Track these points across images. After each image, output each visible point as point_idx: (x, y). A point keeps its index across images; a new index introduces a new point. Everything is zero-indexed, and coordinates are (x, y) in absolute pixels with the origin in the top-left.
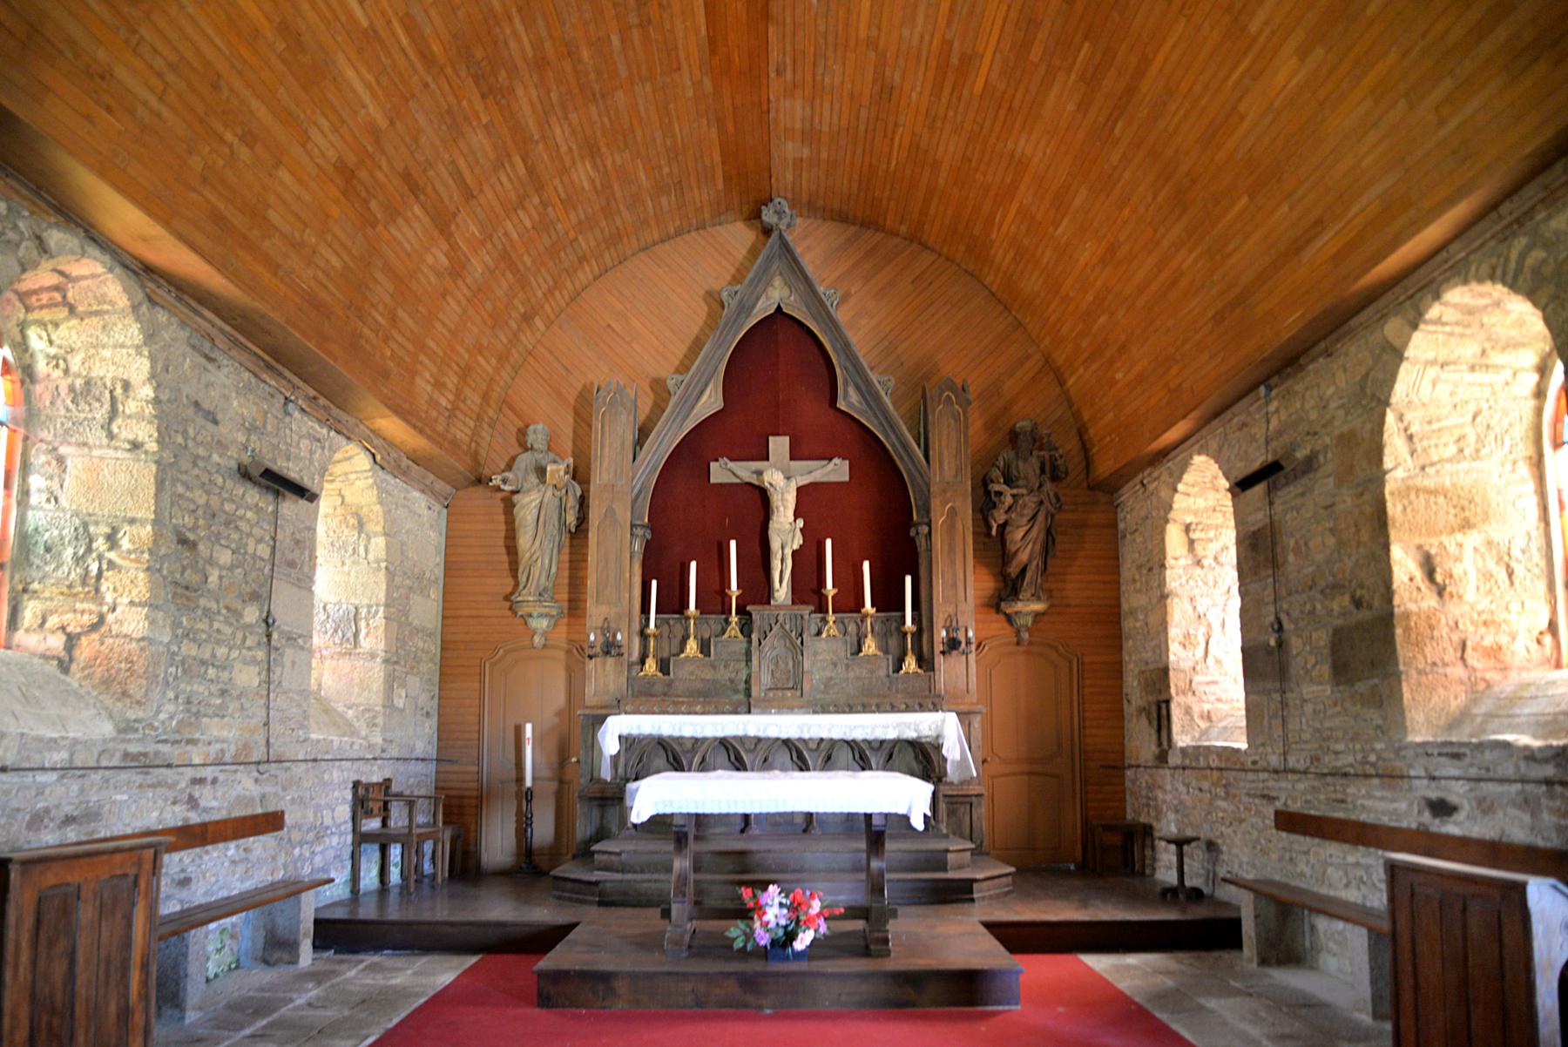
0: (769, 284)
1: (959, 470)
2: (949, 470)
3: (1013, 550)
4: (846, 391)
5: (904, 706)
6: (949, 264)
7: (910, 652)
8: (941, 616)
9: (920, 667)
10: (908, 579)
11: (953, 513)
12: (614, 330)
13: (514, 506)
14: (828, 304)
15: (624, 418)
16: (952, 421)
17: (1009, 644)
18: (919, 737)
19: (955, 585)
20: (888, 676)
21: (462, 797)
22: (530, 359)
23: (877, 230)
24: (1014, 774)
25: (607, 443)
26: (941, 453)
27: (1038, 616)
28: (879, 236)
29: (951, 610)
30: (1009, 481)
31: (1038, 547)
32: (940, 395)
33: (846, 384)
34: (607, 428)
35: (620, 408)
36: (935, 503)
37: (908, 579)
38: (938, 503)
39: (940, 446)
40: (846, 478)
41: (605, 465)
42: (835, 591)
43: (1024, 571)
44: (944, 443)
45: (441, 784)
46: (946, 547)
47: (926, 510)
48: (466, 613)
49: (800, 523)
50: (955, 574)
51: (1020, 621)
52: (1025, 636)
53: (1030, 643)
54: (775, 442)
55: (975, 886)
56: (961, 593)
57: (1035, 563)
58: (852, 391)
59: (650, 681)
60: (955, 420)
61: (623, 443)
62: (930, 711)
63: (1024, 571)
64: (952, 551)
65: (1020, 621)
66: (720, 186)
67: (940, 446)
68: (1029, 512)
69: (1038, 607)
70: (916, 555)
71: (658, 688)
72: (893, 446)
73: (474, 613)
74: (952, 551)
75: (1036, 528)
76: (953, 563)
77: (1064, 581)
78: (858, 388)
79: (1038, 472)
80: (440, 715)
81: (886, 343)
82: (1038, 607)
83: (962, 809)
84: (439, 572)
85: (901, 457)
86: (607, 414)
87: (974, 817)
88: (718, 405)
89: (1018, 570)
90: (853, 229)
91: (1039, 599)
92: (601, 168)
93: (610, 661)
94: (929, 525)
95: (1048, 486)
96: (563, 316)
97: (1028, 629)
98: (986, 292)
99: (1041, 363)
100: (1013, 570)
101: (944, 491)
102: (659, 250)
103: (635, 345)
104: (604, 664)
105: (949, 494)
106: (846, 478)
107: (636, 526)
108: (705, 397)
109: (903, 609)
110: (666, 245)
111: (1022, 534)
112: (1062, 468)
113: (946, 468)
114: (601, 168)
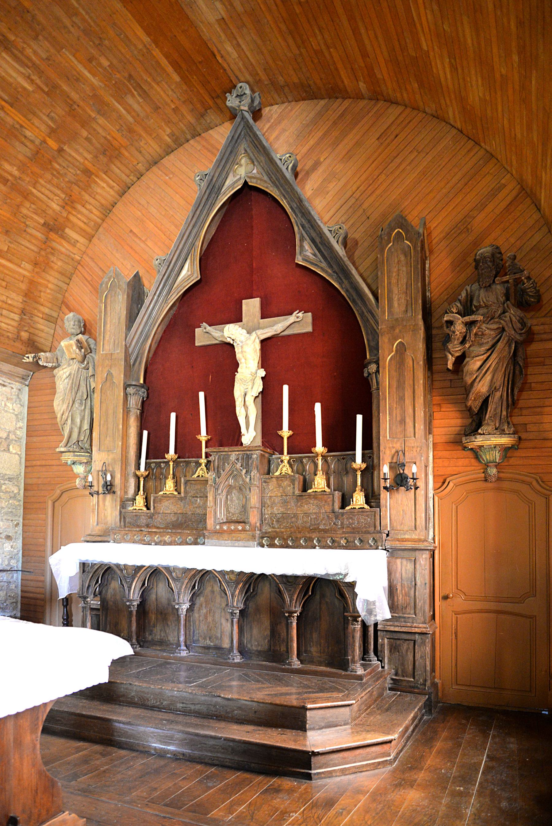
0: (235, 162)
1: (409, 305)
2: (398, 307)
3: (469, 382)
4: (302, 246)
5: (343, 542)
6: (415, 112)
7: (358, 488)
8: (388, 452)
9: (367, 502)
10: (359, 418)
11: (402, 348)
12: (134, 234)
13: (54, 376)
14: (284, 169)
15: (120, 297)
16: (402, 258)
17: (475, 481)
18: (327, 574)
19: (403, 421)
20: (333, 512)
21: (36, 599)
22: (80, 267)
23: (344, 98)
24: (481, 611)
25: (108, 320)
26: (390, 291)
27: (506, 450)
28: (347, 103)
29: (398, 446)
30: (467, 310)
31: (500, 376)
32: (390, 234)
33: (302, 239)
34: (109, 308)
35: (118, 290)
36: (384, 341)
37: (359, 418)
38: (386, 340)
39: (389, 283)
40: (310, 329)
41: (107, 337)
42: (291, 433)
43: (485, 402)
44: (394, 281)
45: (25, 589)
46: (395, 384)
47: (376, 348)
48: (38, 463)
49: (262, 373)
50: (404, 411)
51: (487, 457)
52: (493, 471)
53: (499, 479)
54: (247, 304)
55: (314, 760)
56: (410, 429)
57: (498, 394)
58: (307, 246)
59: (137, 515)
60: (406, 256)
61: (119, 319)
62: (371, 548)
63: (485, 402)
64: (401, 386)
65: (487, 457)
66: (176, 77)
67: (389, 283)
68: (488, 341)
69: (505, 440)
70: (369, 395)
71: (143, 521)
72: (347, 291)
73: (44, 463)
74: (401, 386)
75: (494, 356)
76: (402, 399)
77: (541, 414)
78: (313, 241)
79: (502, 299)
80: (23, 538)
81: (353, 200)
82: (505, 440)
83: (405, 646)
84: (22, 433)
85: (354, 301)
86: (109, 296)
87: (418, 656)
88: (197, 276)
89: (478, 403)
90: (322, 102)
91: (502, 432)
92: (30, 64)
93: (109, 497)
94: (377, 362)
95: (513, 313)
96: (101, 229)
97: (497, 466)
98: (454, 131)
99: (514, 193)
100: (474, 404)
101: (393, 328)
102: (169, 161)
103: (150, 243)
104: (104, 500)
105: (397, 331)
106: (310, 329)
107: (130, 385)
108: (184, 272)
109: (354, 449)
110: (172, 156)
111: (479, 364)
112: (531, 291)
113: (396, 305)
114: (30, 64)
